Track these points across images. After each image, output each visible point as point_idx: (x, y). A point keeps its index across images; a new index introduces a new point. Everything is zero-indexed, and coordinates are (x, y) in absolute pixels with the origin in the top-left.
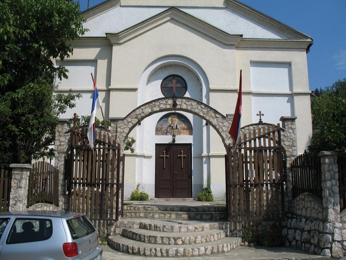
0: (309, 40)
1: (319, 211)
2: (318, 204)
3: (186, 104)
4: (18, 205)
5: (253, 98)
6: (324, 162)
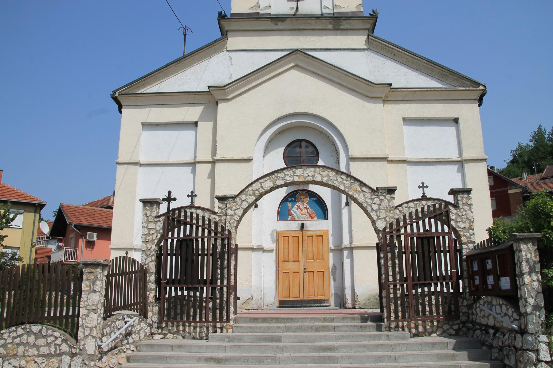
0: (482, 88)
1: (514, 319)
2: (512, 309)
3: (321, 175)
4: (92, 316)
5: (408, 167)
6: (518, 249)
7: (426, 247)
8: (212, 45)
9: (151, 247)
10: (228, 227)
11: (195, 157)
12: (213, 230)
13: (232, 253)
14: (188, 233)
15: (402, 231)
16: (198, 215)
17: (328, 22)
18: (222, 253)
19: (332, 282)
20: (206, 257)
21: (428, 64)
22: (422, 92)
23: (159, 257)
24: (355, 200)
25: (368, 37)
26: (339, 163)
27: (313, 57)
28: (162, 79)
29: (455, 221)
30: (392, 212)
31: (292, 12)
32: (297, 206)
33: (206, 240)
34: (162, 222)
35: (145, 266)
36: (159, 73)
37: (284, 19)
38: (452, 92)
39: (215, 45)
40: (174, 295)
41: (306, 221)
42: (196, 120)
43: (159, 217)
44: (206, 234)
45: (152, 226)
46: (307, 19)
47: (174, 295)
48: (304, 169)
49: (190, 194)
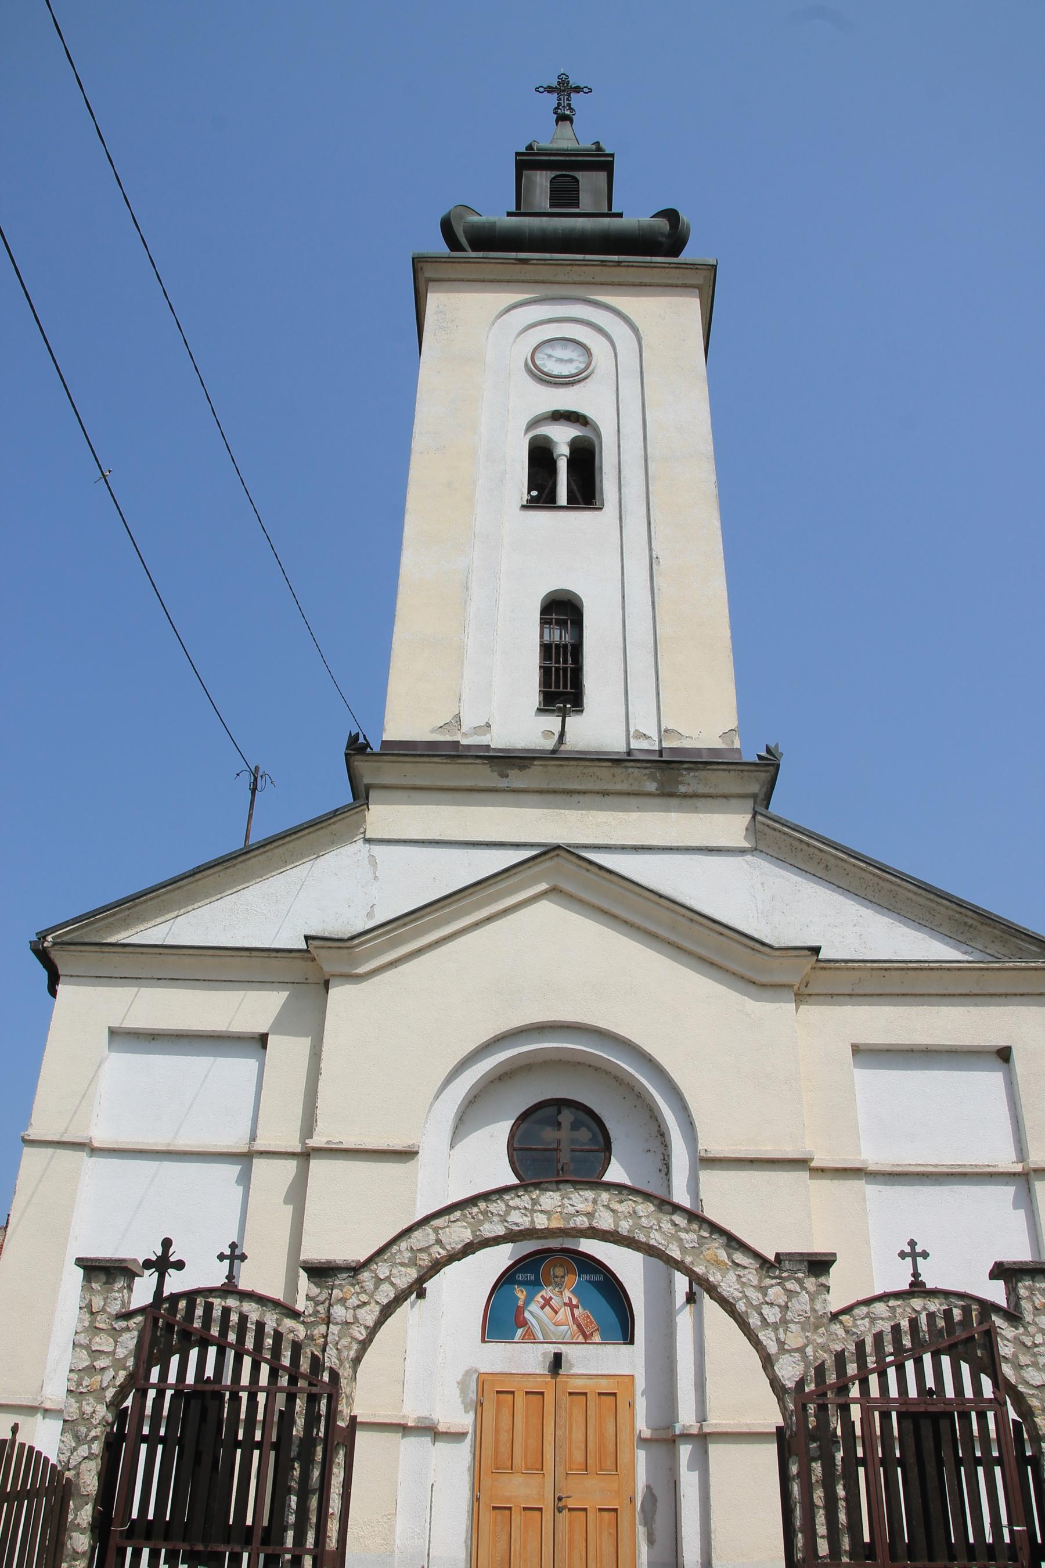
3: (613, 1211)
5: (871, 1190)
7: (928, 1444)
8: (324, 824)
9: (94, 1412)
10: (331, 1359)
11: (253, 1138)
12: (284, 1368)
13: (338, 1444)
14: (209, 1372)
15: (855, 1392)
16: (243, 1318)
17: (645, 775)
18: (308, 1441)
19: (643, 1548)
20: (256, 1453)
21: (920, 895)
22: (904, 972)
23: (112, 1445)
24: (712, 1291)
25: (754, 817)
26: (668, 1173)
27: (601, 867)
28: (180, 909)
29: (1013, 1363)
30: (822, 1330)
31: (549, 744)
32: (542, 1297)
33: (262, 1397)
34: (136, 1333)
35: (68, 1474)
36: (173, 890)
37: (526, 762)
38: (990, 972)
39: (334, 823)
40: (136, 1517)
41: (568, 1346)
42: (264, 1030)
43: (128, 1315)
44: (264, 1380)
45: (102, 1342)
46: (587, 763)
47: (136, 1517)
48: (564, 1192)
49: (228, 1252)
